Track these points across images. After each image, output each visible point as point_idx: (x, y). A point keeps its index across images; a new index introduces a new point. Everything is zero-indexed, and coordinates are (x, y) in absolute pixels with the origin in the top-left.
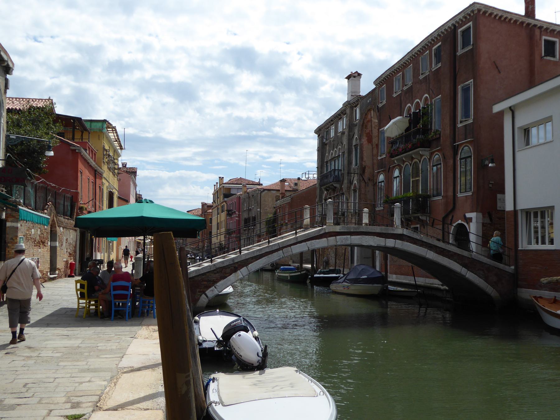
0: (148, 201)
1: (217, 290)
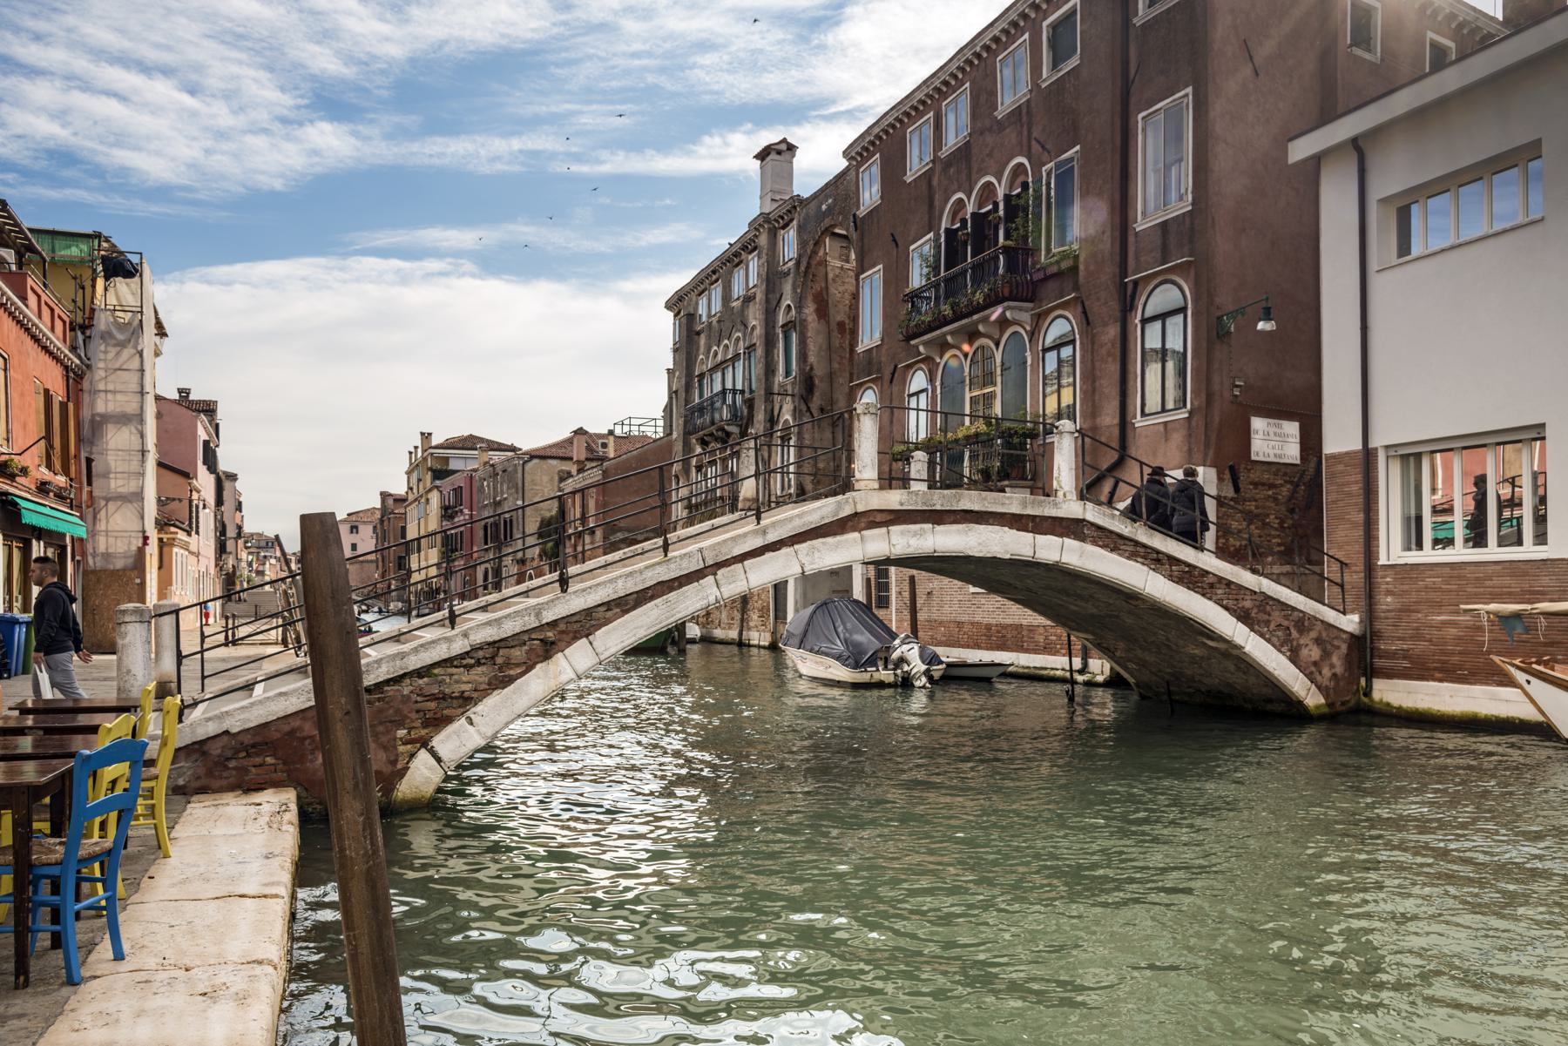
1: (479, 732)
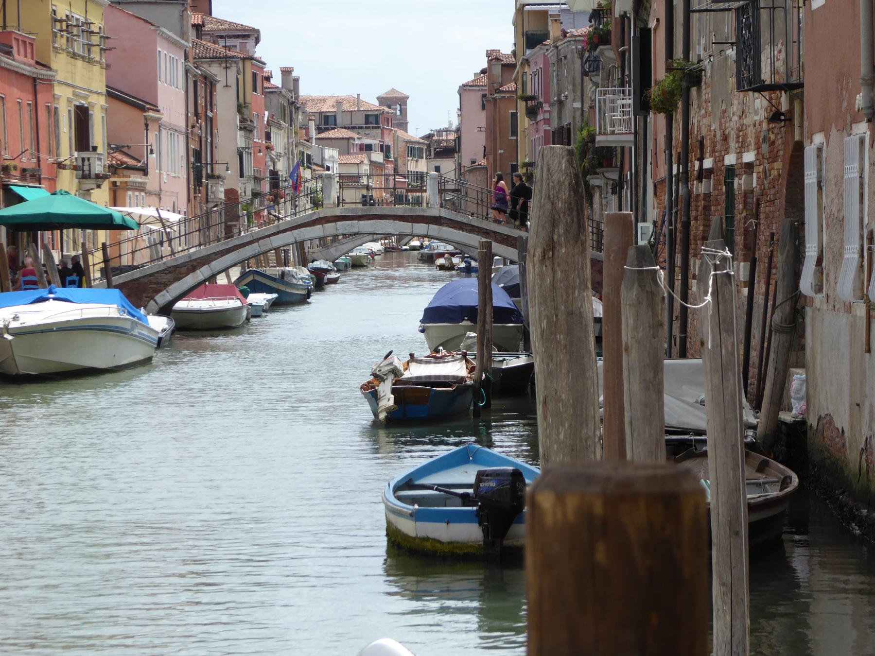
0: (63, 192)
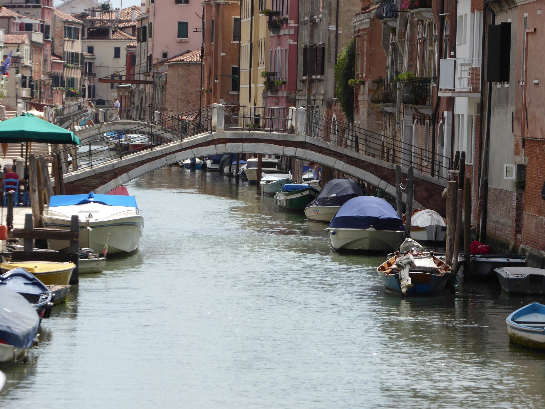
0: (29, 115)
